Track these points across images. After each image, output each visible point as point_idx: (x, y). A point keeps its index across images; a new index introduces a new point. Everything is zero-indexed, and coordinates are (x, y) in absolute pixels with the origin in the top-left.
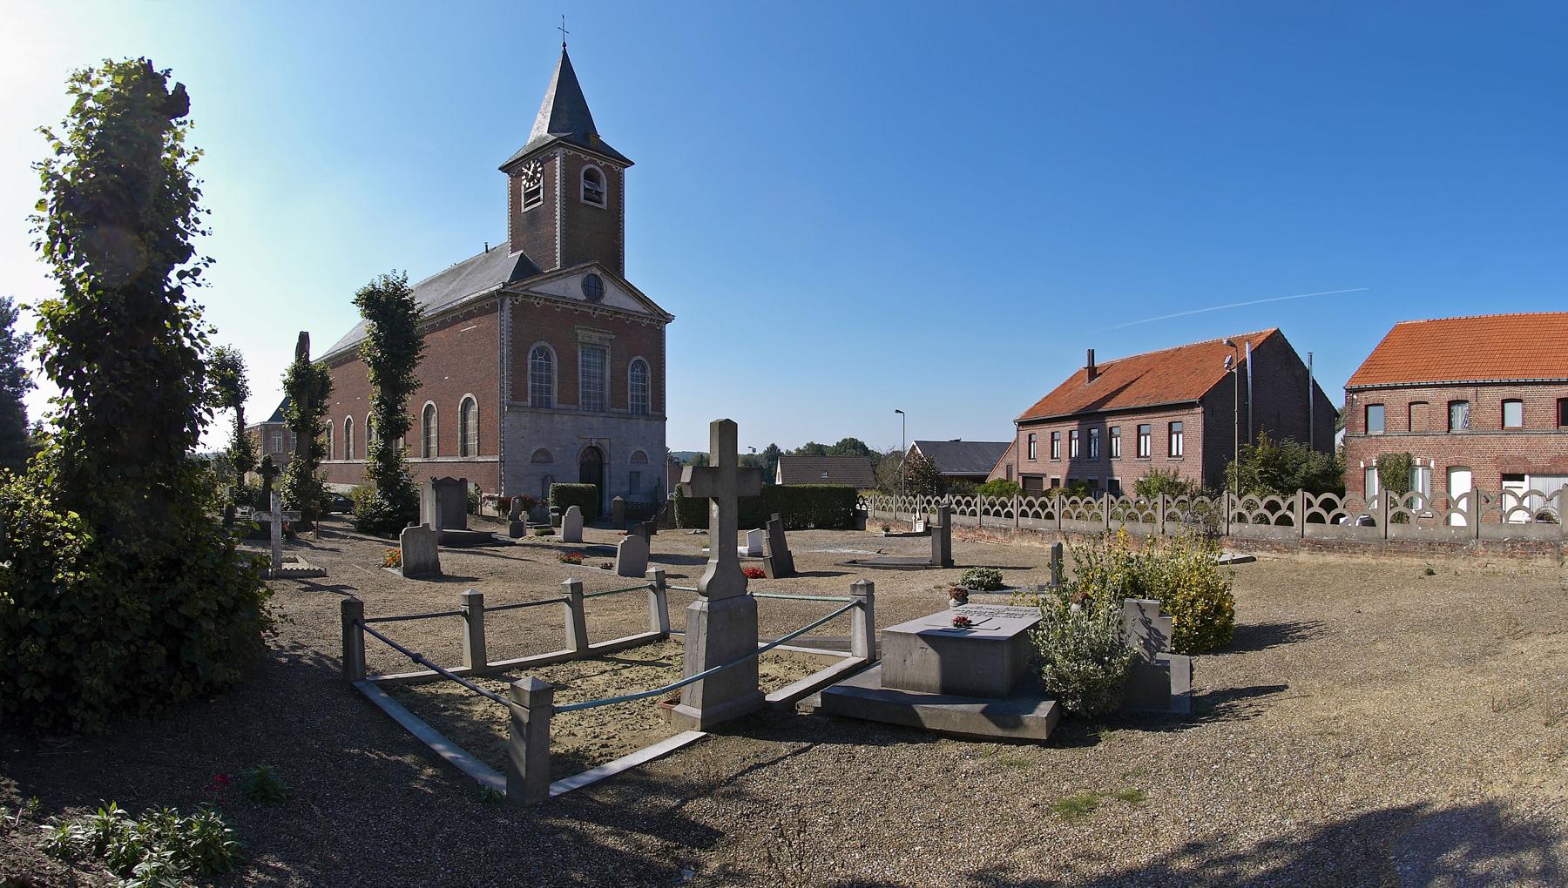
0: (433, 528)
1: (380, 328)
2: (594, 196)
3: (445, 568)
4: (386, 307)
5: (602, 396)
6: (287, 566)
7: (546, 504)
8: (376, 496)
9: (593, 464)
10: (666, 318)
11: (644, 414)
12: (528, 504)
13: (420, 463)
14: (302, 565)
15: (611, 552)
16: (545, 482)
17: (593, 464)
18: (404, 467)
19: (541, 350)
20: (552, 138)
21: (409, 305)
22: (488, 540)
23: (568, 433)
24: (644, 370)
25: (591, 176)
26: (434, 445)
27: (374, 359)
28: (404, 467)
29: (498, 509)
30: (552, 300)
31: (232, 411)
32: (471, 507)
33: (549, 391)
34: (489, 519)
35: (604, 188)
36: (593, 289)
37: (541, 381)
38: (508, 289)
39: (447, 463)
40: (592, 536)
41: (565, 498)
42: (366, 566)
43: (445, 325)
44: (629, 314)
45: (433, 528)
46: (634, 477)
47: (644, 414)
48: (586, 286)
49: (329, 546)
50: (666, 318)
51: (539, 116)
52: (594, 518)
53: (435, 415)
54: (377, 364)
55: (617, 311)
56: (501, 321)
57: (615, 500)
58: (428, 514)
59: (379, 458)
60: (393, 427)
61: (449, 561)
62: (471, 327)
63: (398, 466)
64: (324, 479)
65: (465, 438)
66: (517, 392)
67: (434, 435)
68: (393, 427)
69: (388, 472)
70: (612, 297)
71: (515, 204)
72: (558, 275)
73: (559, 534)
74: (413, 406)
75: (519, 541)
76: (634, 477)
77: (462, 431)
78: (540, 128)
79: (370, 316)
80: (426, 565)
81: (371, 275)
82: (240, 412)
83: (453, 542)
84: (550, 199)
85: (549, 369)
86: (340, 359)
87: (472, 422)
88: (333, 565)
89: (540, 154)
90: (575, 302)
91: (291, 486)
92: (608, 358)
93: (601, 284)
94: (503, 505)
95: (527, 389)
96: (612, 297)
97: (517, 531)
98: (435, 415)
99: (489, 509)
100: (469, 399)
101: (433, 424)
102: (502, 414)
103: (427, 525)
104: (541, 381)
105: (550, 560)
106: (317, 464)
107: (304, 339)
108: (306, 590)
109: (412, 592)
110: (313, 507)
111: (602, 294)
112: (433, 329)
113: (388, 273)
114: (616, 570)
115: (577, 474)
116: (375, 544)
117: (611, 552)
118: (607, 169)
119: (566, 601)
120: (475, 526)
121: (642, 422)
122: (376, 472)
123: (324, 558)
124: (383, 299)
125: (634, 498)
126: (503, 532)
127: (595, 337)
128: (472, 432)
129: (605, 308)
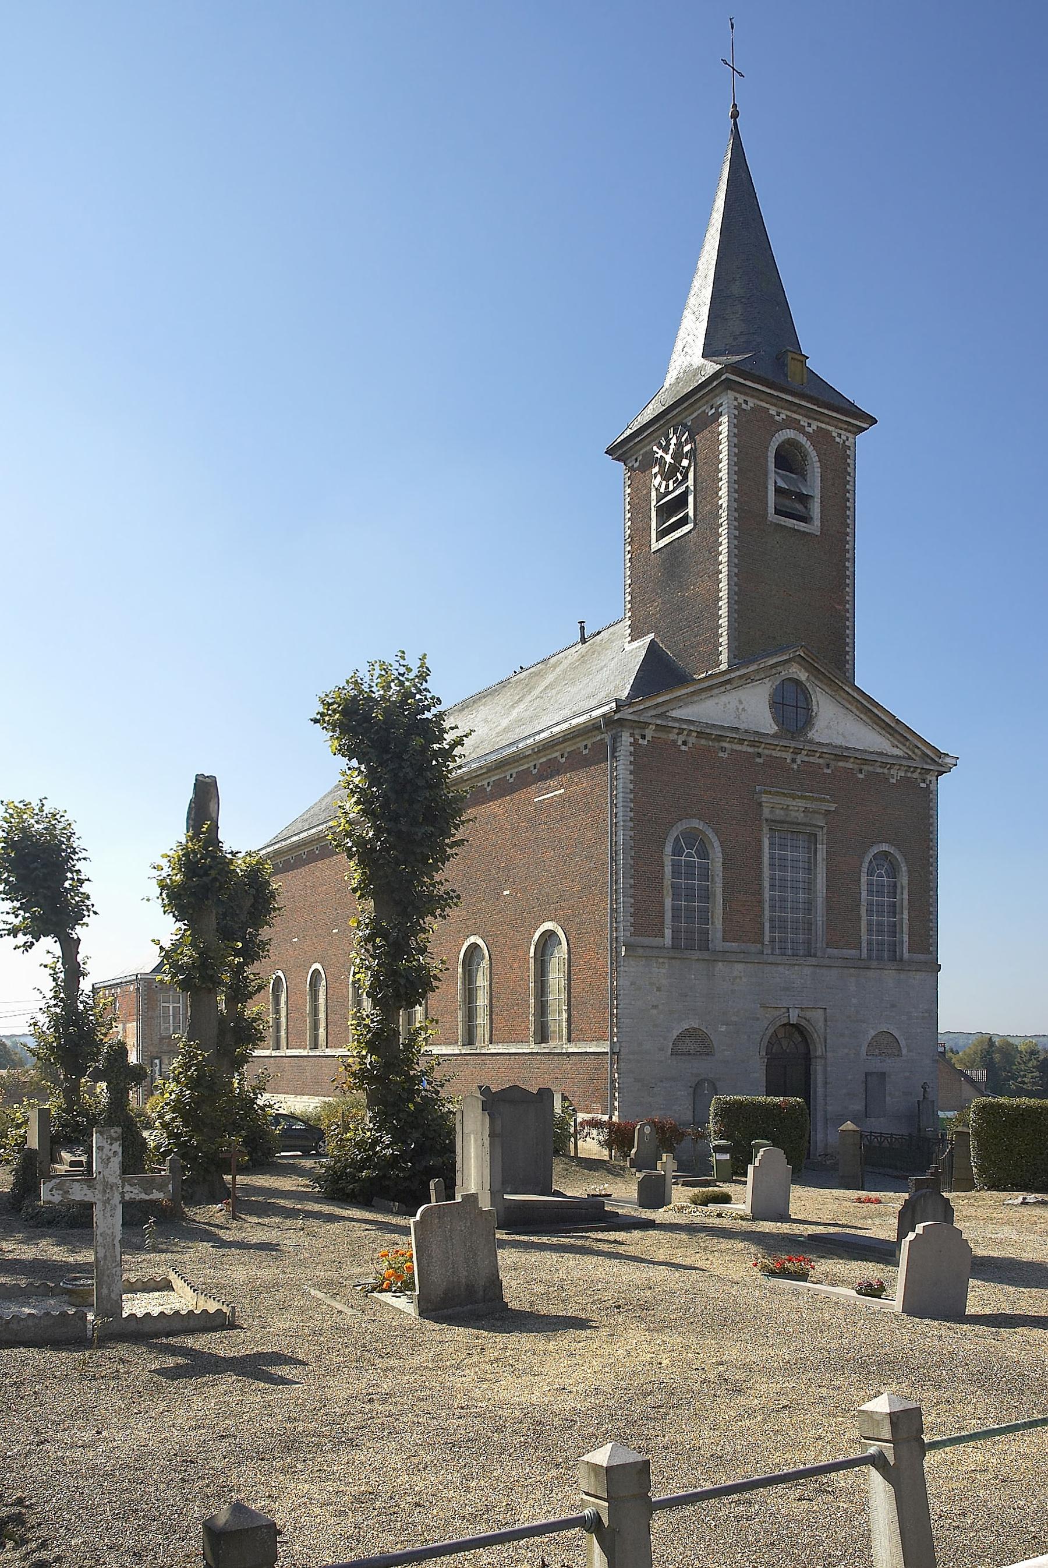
0: (485, 1204)
1: (372, 777)
2: (794, 504)
3: (516, 1293)
4: (388, 736)
5: (809, 926)
6: (139, 1305)
7: (704, 1136)
8: (366, 1124)
9: (792, 1058)
10: (936, 763)
11: (895, 958)
12: (667, 1137)
13: (459, 1055)
14: (182, 1300)
15: (882, 1252)
16: (701, 1090)
17: (792, 1058)
18: (423, 1065)
19: (691, 838)
20: (712, 367)
21: (433, 730)
22: (593, 1215)
23: (743, 997)
24: (893, 872)
25: (789, 460)
26: (482, 1020)
27: (361, 842)
28: (423, 1065)
29: (608, 1144)
30: (706, 733)
31: (49, 946)
32: (557, 1141)
33: (705, 917)
34: (592, 1165)
35: (814, 486)
36: (792, 709)
37: (690, 897)
38: (626, 714)
39: (509, 1056)
40: (815, 1206)
41: (744, 1127)
42: (332, 1287)
43: (502, 789)
44: (864, 759)
45: (485, 1204)
46: (874, 1083)
47: (895, 958)
48: (778, 705)
49: (258, 1236)
50: (936, 763)
51: (697, 283)
52: (811, 1167)
53: (485, 964)
54: (366, 854)
55: (841, 754)
56: (612, 782)
57: (839, 1129)
58: (474, 1172)
59: (372, 1046)
60: (400, 984)
61: (526, 1272)
62: (553, 792)
63: (410, 1062)
64: (260, 1089)
65: (542, 1008)
66: (644, 920)
67: (482, 1000)
68: (400, 984)
69: (391, 1076)
70: (833, 725)
71: (638, 536)
72: (724, 683)
73: (742, 1200)
74: (446, 941)
75: (659, 1215)
76: (874, 1083)
77: (537, 991)
78: (688, 355)
79: (349, 752)
80: (470, 1289)
81: (352, 657)
82: (70, 947)
83: (525, 1222)
84: (707, 520)
85: (706, 874)
86: (300, 854)
87: (556, 978)
88: (256, 1289)
89: (688, 412)
90: (757, 738)
91: (178, 1107)
92: (822, 850)
93: (808, 699)
94: (619, 1138)
95: (668, 908)
96: (833, 725)
97: (654, 1194)
98: (485, 964)
99: (591, 1146)
100: (549, 935)
101: (482, 980)
102: (616, 961)
103: (471, 1199)
104: (690, 897)
105: (735, 1268)
106: (245, 1059)
107: (205, 796)
108: (173, 1374)
109: (437, 1365)
110: (222, 1151)
111: (809, 721)
112: (481, 797)
113: (390, 659)
114: (896, 1300)
115: (759, 1074)
116: (359, 1231)
117: (882, 1252)
118: (821, 439)
119: (878, 1461)
120: (575, 1188)
121: (889, 975)
122: (363, 1077)
123: (240, 1271)
124: (378, 714)
125: (878, 1125)
126: (623, 1193)
127: (797, 808)
128: (556, 995)
129: (816, 749)
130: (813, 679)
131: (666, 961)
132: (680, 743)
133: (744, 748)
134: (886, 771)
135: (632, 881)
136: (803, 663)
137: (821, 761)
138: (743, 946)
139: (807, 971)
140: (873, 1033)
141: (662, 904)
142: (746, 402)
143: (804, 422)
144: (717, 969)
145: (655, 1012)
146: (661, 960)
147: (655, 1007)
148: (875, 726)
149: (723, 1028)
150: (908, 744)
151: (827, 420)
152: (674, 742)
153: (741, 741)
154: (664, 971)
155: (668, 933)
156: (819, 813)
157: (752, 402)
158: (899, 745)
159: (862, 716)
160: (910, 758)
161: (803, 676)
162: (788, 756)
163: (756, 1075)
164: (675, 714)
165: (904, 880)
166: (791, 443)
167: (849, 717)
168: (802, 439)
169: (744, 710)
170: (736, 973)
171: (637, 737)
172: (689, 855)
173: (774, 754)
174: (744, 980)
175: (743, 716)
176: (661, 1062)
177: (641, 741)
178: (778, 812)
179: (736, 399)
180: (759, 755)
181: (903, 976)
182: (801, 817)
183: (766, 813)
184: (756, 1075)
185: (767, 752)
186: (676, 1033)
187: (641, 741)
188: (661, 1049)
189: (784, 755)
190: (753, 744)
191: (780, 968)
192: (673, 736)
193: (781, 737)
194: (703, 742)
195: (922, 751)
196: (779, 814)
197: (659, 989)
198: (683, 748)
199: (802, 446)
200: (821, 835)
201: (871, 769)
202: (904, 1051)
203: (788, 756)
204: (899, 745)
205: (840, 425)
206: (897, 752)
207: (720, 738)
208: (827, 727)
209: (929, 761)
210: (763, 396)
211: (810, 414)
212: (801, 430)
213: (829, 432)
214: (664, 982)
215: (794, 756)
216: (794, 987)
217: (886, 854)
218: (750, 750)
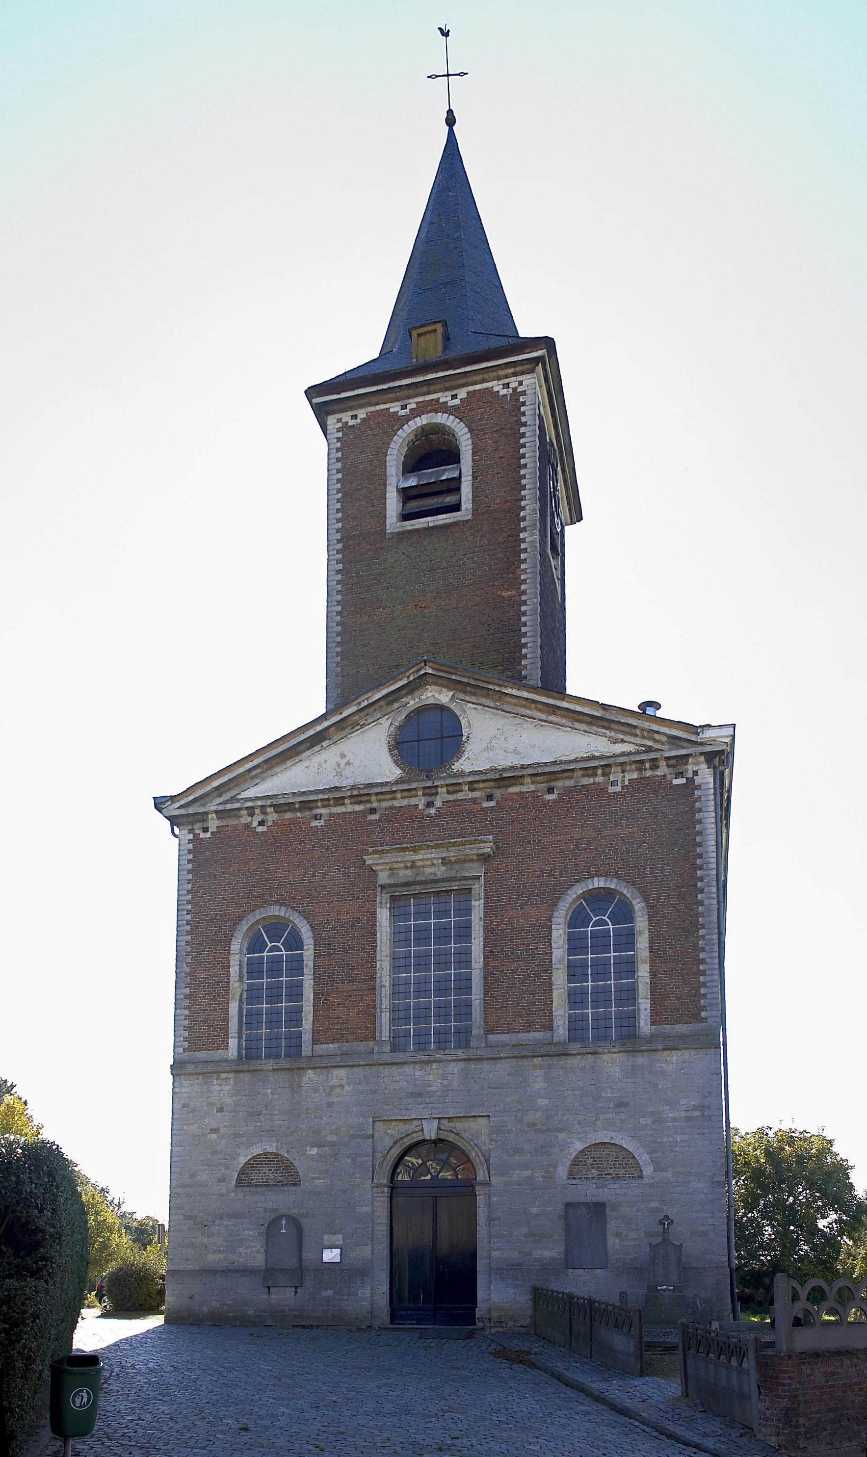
19: (276, 928)
44: (550, 774)
47: (629, 1038)
48: (401, 746)
55: (504, 779)
76: (586, 1220)
90: (385, 791)
92: (478, 907)
121: (613, 1064)
130: (462, 696)
131: (231, 1076)
132: (255, 824)
133: (350, 808)
134: (600, 779)
135: (187, 991)
136: (439, 681)
137: (477, 794)
138: (346, 1046)
139: (455, 1068)
140: (579, 1146)
141: (226, 1011)
142: (354, 417)
143: (444, 397)
144: (305, 1079)
145: (214, 1136)
146: (224, 1076)
147: (214, 1131)
148: (577, 725)
149: (314, 1151)
150: (638, 732)
151: (425, 389)
152: (247, 826)
153: (339, 801)
154: (228, 1088)
155: (233, 1043)
156: (472, 861)
157: (362, 414)
158: (627, 738)
159: (551, 718)
160: (649, 749)
161: (444, 697)
162: (420, 802)
163: (365, 1209)
164: (244, 795)
165: (641, 923)
166: (425, 432)
167: (526, 725)
168: (441, 418)
169: (348, 763)
170: (334, 1081)
171: (197, 831)
172: (273, 949)
173: (396, 803)
174: (347, 1088)
175: (347, 772)
176: (222, 1195)
177: (202, 835)
178: (402, 873)
179: (339, 420)
180: (373, 811)
181: (641, 1060)
182: (441, 871)
183: (383, 878)
184: (365, 1209)
185: (385, 804)
186: (242, 1160)
187: (202, 835)
188: (221, 1180)
189: (413, 801)
190: (356, 798)
191: (408, 1069)
192: (245, 819)
193: (409, 781)
194: (288, 815)
195: (665, 734)
196: (406, 875)
197: (221, 1110)
198: (260, 829)
199: (444, 426)
200: (478, 888)
201: (569, 783)
202: (648, 1171)
203: (420, 802)
204: (627, 738)
205: (502, 373)
206: (620, 748)
207: (307, 805)
208: (487, 749)
209: (685, 744)
210: (374, 399)
211: (448, 384)
212: (443, 408)
213: (489, 391)
214: (228, 1101)
215: (430, 799)
216: (429, 1093)
217: (608, 894)
218: (358, 808)
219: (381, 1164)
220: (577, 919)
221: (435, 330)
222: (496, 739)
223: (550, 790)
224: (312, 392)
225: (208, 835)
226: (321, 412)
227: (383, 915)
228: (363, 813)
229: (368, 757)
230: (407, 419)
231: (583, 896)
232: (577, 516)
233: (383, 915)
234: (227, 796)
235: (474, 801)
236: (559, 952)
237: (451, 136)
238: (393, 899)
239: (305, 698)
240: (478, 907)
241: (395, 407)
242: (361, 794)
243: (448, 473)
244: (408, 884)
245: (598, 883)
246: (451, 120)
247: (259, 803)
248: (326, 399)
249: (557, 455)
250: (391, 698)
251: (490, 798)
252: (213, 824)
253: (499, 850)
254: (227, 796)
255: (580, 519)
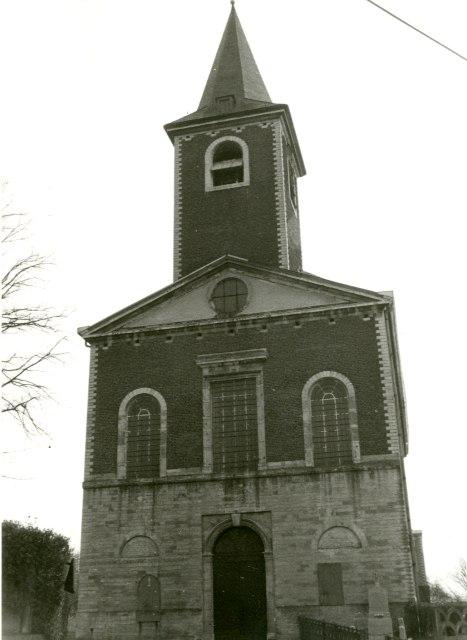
92: (260, 388)
121: (339, 483)
143: (234, 129)
157: (192, 136)
182: (238, 369)
196: (218, 371)
200: (260, 378)
212: (233, 134)
219: (207, 542)
220: (316, 394)
221: (314, 531)
222: (265, 300)
223: (297, 324)
224: (167, 127)
225: (106, 348)
226: (172, 135)
227: (206, 393)
228: (195, 336)
229: (198, 308)
230: (215, 138)
231: (319, 381)
232: (302, 172)
233: (206, 393)
234: (118, 327)
235: (255, 329)
236: (307, 417)
237: (233, 10)
238: (211, 384)
239: (163, 275)
240: (260, 388)
241: (209, 133)
242: (192, 327)
243: (236, 164)
244: (220, 375)
245: (326, 374)
246: (233, 3)
247: (137, 331)
248: (174, 130)
249: (292, 147)
250: (209, 275)
251: (264, 328)
252: (110, 342)
253: (271, 357)
254: (118, 327)
255: (304, 173)
